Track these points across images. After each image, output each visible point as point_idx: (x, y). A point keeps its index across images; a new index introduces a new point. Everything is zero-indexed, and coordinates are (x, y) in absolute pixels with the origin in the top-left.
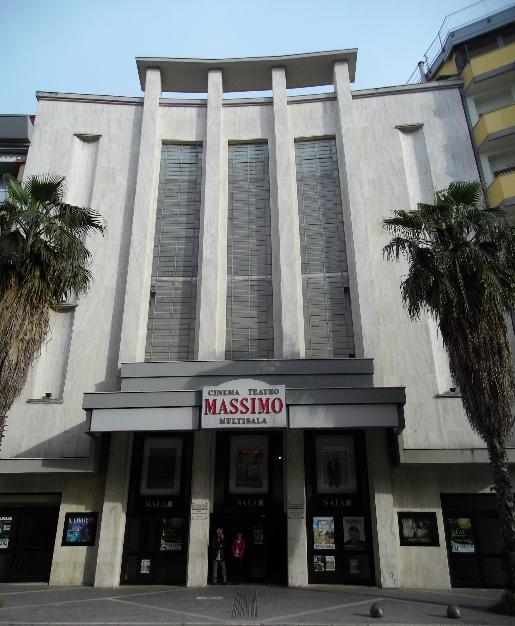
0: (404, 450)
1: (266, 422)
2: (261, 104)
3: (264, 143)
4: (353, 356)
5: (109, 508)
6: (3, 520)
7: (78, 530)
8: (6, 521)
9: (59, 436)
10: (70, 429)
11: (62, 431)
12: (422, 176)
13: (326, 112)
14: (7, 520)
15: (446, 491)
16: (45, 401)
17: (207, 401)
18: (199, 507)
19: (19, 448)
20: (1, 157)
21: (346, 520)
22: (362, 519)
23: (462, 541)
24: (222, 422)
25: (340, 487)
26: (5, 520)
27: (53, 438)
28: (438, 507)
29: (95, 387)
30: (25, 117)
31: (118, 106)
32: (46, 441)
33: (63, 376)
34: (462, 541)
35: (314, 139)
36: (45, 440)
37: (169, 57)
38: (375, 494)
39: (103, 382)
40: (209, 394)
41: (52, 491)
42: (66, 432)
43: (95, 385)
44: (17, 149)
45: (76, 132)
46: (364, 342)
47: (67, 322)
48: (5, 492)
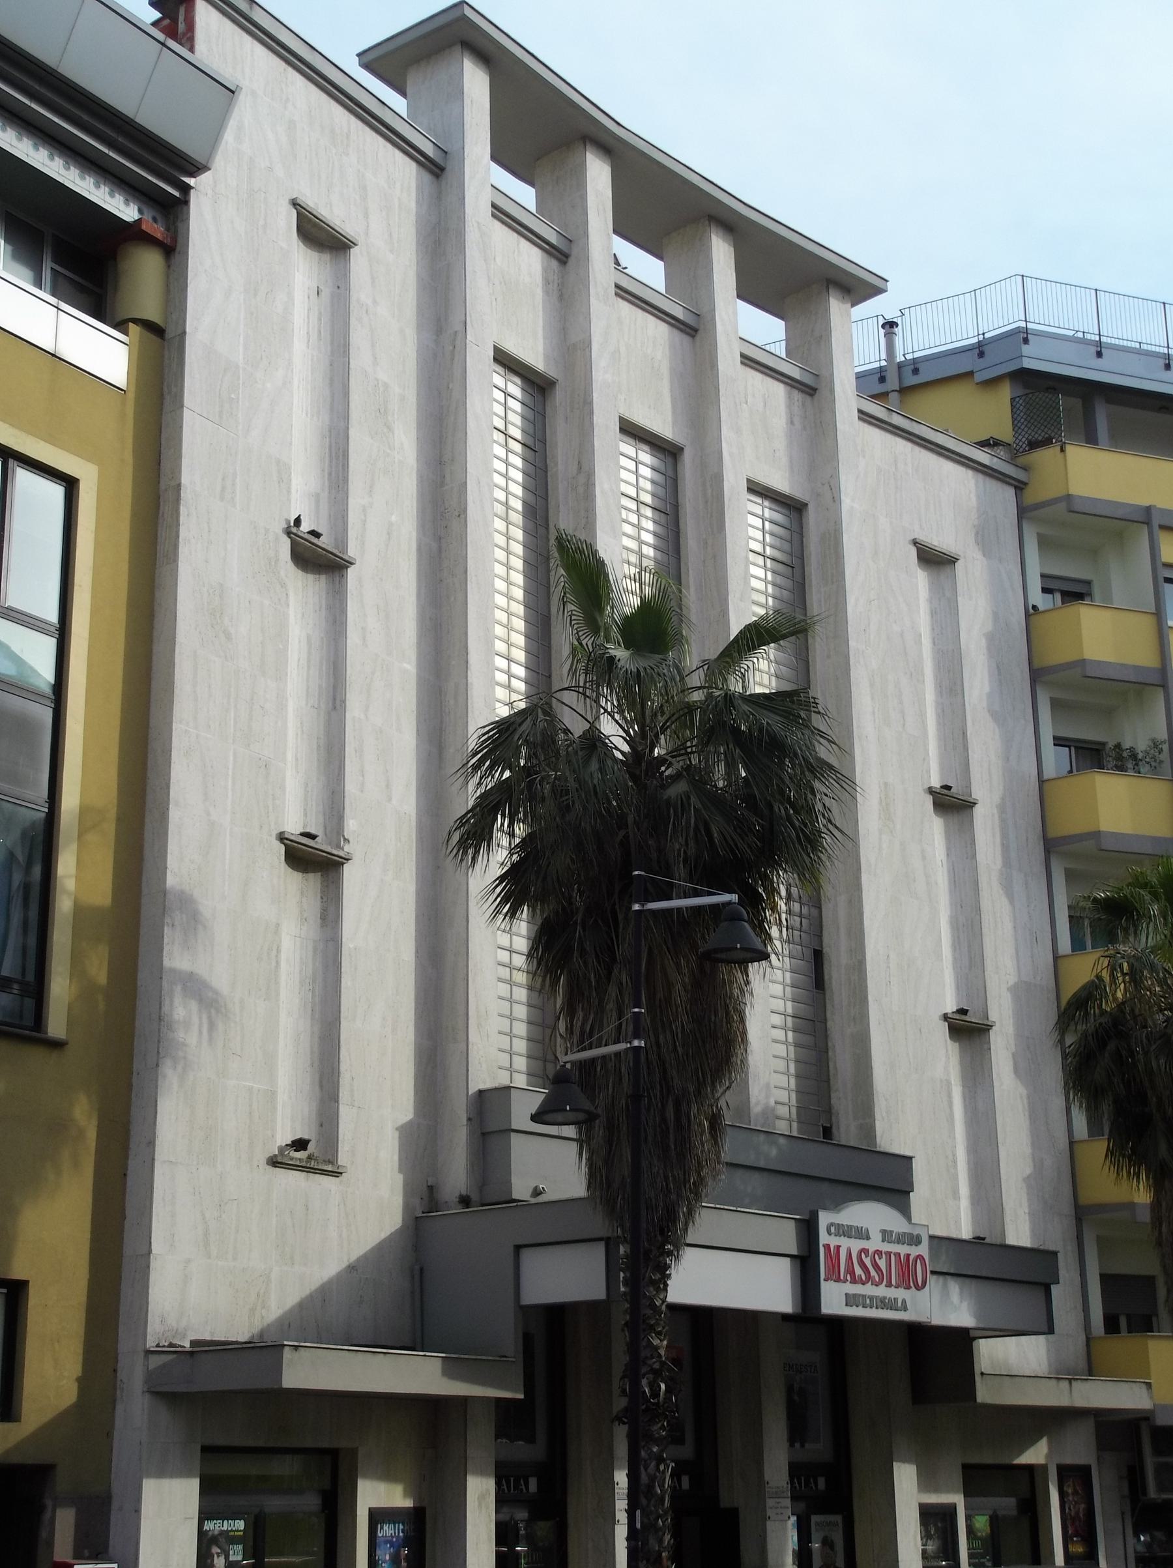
0: (982, 1374)
1: (905, 1309)
2: (682, 326)
3: (668, 451)
4: (827, 1132)
5: (477, 1496)
6: (228, 1531)
7: (387, 1557)
8: (232, 1533)
9: (339, 1276)
10: (358, 1260)
11: (345, 1264)
12: (942, 696)
13: (792, 423)
14: (234, 1529)
15: (976, 1459)
16: (312, 1166)
17: (827, 1247)
18: (776, 1492)
19: (264, 1307)
20: (4, 130)
21: (817, 1524)
22: (838, 1519)
23: (977, 1561)
24: (851, 1300)
25: (807, 1446)
26: (230, 1529)
27: (330, 1282)
28: (957, 1492)
29: (397, 1134)
30: (233, 92)
31: (640, 311)
32: (316, 1291)
33: (321, 1086)
34: (977, 1561)
35: (763, 492)
36: (313, 1288)
37: (535, 54)
38: (894, 1463)
39: (410, 1123)
40: (829, 1233)
41: (287, 1445)
42: (352, 1268)
43: (397, 1129)
44: (150, 178)
45: (311, 201)
46: (876, 1109)
47: (313, 905)
48: (251, 1443)
